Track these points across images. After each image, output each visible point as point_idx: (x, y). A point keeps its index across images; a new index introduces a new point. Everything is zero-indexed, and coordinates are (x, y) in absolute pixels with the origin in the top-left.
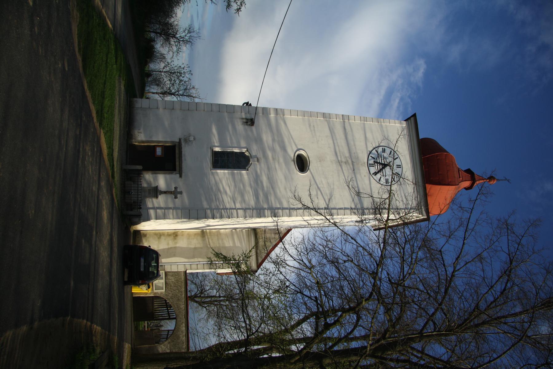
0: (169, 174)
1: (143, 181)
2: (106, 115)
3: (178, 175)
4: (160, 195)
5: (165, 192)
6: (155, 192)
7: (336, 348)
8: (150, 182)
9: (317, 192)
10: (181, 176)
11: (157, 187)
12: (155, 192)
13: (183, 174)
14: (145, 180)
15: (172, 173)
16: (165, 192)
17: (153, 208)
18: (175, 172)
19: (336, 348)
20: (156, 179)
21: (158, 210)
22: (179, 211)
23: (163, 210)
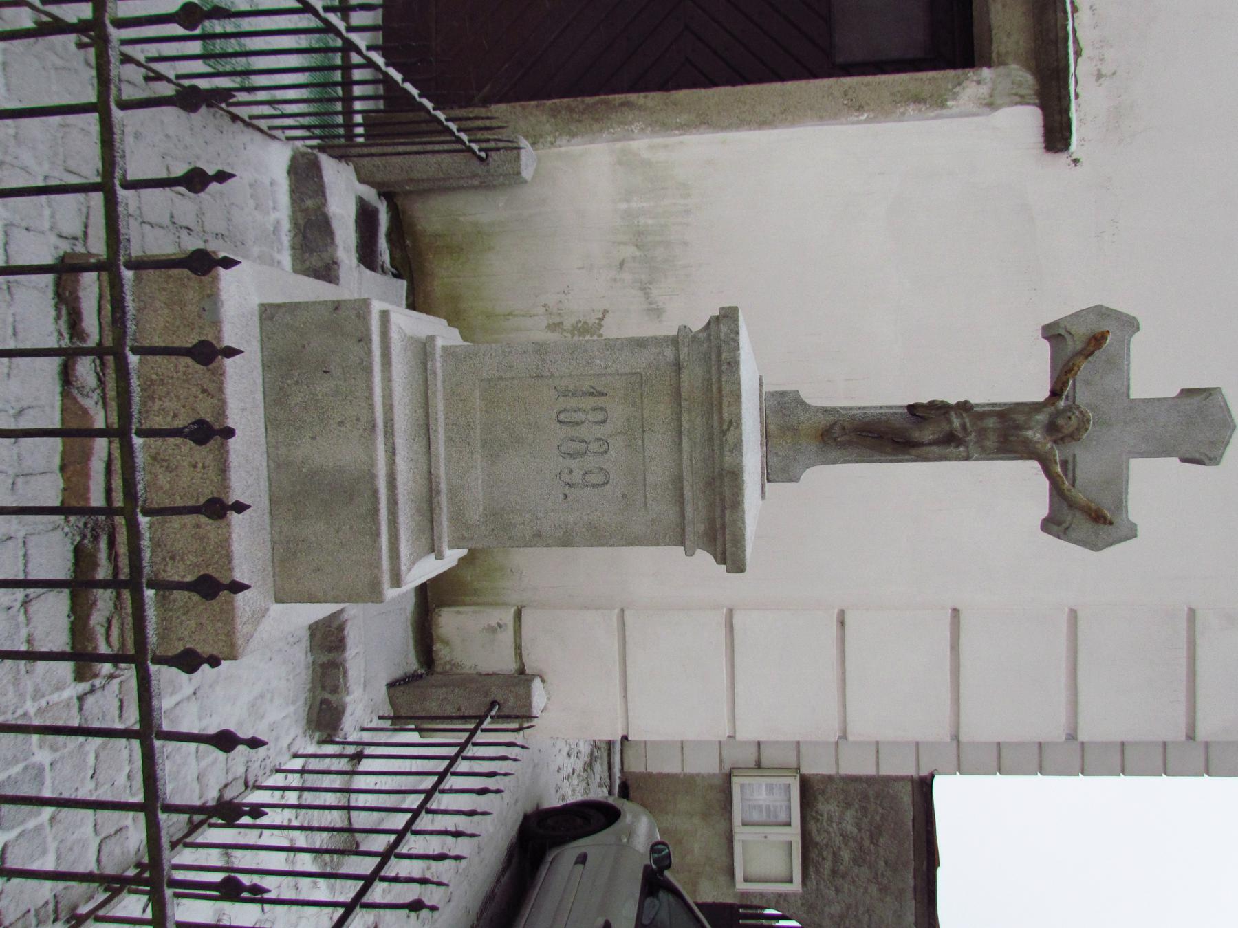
3: (1026, 121)
18: (976, 84)
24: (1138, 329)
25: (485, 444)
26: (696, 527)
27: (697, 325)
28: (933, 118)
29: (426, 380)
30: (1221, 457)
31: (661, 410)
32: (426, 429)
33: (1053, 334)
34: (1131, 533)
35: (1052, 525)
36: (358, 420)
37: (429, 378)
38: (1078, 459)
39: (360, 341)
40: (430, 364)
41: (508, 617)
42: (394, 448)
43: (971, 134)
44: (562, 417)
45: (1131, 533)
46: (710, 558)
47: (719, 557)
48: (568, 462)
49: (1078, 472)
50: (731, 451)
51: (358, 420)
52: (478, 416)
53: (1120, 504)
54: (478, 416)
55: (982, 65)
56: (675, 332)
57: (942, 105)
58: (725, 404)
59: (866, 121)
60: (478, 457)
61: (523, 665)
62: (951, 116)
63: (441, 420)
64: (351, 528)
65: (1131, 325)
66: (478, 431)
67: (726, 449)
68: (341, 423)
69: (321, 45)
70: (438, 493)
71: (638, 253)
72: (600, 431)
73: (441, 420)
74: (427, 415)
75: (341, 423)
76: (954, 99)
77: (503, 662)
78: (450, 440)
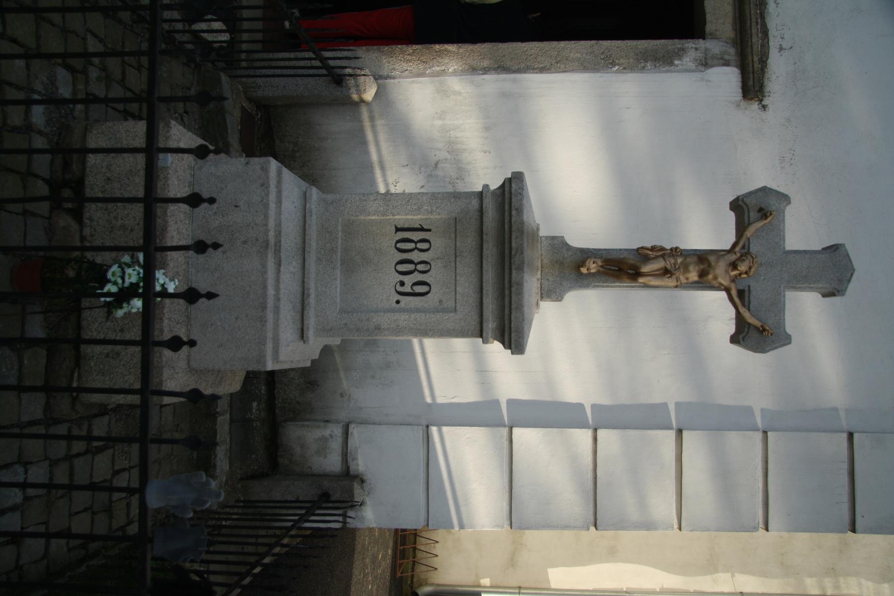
0: (639, 63)
1: (381, 147)
2: (413, 316)
3: (727, 78)
4: (552, 293)
5: (621, 268)
6: (495, 259)
7: (205, 35)
8: (454, 148)
9: (20, 45)
10: (753, 88)
11: (510, 195)
12: (495, 259)
13: (778, 67)
14: (403, 132)
15: (666, 61)
16: (621, 268)
17: (482, 414)
18: (693, 48)
19: (205, 35)
20: (510, 126)
21: (527, 438)
22: (744, 447)
23: (583, 436)
24: (790, 203)
25: (343, 262)
26: (490, 325)
27: (495, 185)
28: (664, 72)
29: (305, 217)
30: (845, 290)
31: (469, 242)
32: (303, 251)
33: (737, 206)
34: (786, 340)
35: (734, 339)
36: (257, 240)
37: (307, 215)
38: (751, 289)
39: (262, 186)
40: (308, 205)
41: (338, 431)
42: (280, 261)
43: (691, 89)
44: (399, 245)
45: (786, 340)
46: (501, 345)
47: (506, 343)
48: (402, 278)
49: (752, 298)
50: (517, 269)
51: (257, 240)
52: (340, 243)
53: (781, 323)
54: (340, 243)
55: (699, 38)
56: (480, 189)
57: (671, 63)
58: (513, 237)
59: (616, 72)
60: (338, 272)
61: (348, 467)
62: (678, 71)
63: (314, 244)
64: (247, 316)
65: (785, 198)
66: (339, 254)
67: (513, 267)
68: (245, 242)
69: (173, 24)
70: (309, 295)
71: (449, 157)
72: (424, 256)
73: (314, 244)
74: (304, 242)
75: (245, 242)
76: (680, 59)
77: (332, 463)
78: (319, 259)
